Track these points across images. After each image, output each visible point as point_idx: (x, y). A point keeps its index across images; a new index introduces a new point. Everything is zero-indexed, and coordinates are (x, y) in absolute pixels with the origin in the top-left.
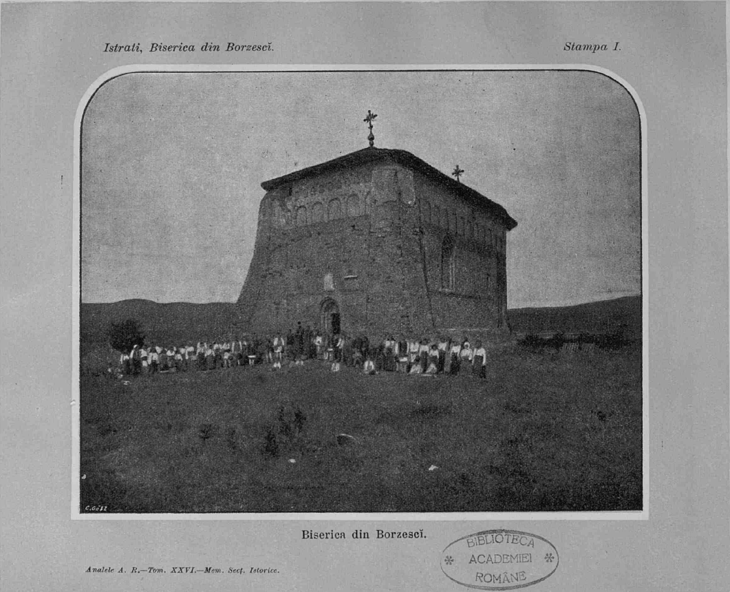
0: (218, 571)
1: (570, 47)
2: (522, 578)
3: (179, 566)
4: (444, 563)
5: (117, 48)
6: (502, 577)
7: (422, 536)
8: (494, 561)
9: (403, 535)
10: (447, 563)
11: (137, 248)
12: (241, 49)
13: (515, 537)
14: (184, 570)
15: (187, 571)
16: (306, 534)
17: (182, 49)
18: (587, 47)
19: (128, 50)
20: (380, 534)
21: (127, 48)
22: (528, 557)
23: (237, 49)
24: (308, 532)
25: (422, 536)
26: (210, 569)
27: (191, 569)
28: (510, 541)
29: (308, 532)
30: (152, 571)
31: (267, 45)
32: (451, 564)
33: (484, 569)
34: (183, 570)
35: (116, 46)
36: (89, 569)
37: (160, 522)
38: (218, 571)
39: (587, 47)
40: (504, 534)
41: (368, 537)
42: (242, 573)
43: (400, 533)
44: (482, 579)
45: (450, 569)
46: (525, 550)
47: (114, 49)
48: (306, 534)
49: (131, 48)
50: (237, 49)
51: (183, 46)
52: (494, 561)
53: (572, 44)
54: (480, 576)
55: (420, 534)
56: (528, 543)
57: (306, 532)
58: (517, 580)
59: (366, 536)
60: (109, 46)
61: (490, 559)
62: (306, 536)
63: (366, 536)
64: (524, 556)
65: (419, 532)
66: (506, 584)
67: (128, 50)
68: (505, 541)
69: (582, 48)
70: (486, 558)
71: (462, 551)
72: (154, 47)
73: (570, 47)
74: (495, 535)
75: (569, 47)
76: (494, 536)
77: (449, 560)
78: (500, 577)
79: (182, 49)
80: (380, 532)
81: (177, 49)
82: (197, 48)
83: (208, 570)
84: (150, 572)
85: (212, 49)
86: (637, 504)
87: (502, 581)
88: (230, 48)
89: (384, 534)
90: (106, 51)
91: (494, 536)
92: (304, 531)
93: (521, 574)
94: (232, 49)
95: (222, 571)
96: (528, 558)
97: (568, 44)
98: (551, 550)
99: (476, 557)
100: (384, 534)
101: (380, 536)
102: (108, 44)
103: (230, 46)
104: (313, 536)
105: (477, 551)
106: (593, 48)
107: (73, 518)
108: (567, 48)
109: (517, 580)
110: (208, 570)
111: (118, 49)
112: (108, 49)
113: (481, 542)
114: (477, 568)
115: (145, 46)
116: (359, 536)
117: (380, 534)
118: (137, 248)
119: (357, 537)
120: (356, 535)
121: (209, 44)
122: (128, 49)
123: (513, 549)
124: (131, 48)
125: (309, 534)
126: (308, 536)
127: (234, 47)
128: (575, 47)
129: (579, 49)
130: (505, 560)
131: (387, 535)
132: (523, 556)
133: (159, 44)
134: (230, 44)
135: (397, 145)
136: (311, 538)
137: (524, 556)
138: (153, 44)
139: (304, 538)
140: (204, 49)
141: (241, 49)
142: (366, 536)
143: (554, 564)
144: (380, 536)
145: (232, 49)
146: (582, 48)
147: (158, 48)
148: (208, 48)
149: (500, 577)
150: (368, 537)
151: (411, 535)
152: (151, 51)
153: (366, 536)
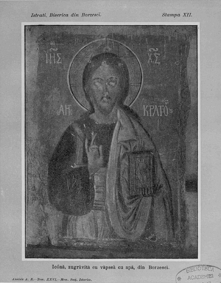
0: (66, 280)
1: (33, 15)
3: (50, 278)
5: (36, 15)
7: (167, 269)
8: (198, 278)
9: (160, 268)
10: (178, 280)
12: (88, 16)
13: (206, 268)
14: (52, 279)
15: (53, 280)
17: (63, 15)
18: (172, 15)
20: (150, 267)
23: (86, 16)
28: (204, 269)
30: (39, 279)
35: (36, 15)
38: (66, 280)
39: (172, 15)
41: (115, 269)
42: (76, 281)
46: (211, 273)
47: (35, 16)
49: (42, 15)
50: (86, 16)
51: (63, 14)
52: (198, 278)
53: (166, 14)
55: (167, 268)
56: (211, 269)
59: (143, 268)
60: (33, 14)
61: (196, 277)
63: (144, 268)
64: (210, 275)
65: (166, 267)
68: (202, 269)
69: (170, 15)
72: (51, 15)
73: (165, 15)
76: (197, 268)
79: (63, 15)
80: (150, 266)
81: (61, 16)
83: (62, 280)
84: (38, 280)
85: (76, 15)
88: (83, 16)
90: (32, 17)
91: (197, 268)
92: (149, 266)
94: (52, 16)
97: (164, 14)
99: (190, 277)
100: (152, 267)
101: (150, 268)
102: (33, 14)
103: (84, 15)
105: (190, 274)
106: (174, 15)
108: (163, 15)
110: (62, 280)
112: (33, 16)
113: (192, 270)
116: (140, 268)
117: (150, 267)
119: (140, 268)
120: (139, 267)
121: (167, 14)
122: (41, 16)
124: (42, 15)
127: (85, 15)
128: (167, 15)
132: (210, 275)
138: (83, 14)
140: (72, 16)
141: (88, 16)
142: (143, 268)
143: (178, 276)
144: (150, 268)
145: (52, 16)
146: (170, 15)
150: (144, 269)
152: (32, 17)
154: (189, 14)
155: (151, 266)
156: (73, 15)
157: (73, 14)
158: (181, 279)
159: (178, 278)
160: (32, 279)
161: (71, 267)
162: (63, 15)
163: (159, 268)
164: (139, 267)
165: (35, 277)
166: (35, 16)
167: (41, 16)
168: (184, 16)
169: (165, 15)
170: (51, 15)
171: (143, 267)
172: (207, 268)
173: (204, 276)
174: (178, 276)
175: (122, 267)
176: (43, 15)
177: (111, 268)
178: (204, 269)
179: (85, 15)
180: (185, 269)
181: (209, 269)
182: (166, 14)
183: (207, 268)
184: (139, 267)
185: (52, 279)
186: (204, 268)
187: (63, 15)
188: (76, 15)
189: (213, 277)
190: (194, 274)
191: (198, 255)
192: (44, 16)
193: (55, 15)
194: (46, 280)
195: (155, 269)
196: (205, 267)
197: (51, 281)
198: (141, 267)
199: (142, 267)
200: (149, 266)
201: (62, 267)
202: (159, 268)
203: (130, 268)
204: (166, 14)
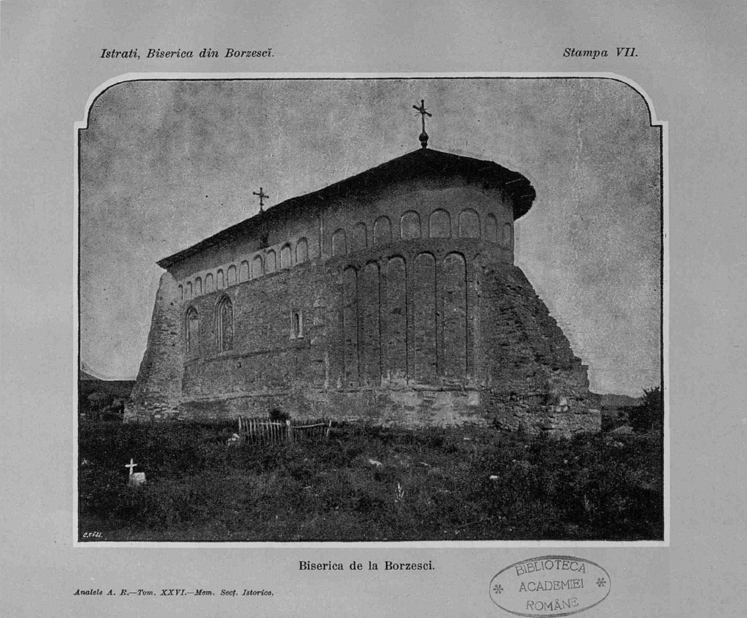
1: (570, 52)
2: (574, 604)
4: (493, 593)
6: (554, 604)
7: (430, 568)
8: (544, 588)
14: (174, 592)
16: (303, 565)
17: (180, 54)
18: (588, 53)
19: (203, 56)
22: (580, 583)
24: (305, 563)
25: (430, 568)
26: (201, 591)
29: (305, 563)
30: (142, 593)
32: (500, 592)
34: (173, 592)
35: (113, 52)
36: (78, 591)
37: (97, 549)
41: (342, 569)
43: (409, 565)
44: (533, 606)
48: (303, 565)
49: (129, 54)
52: (544, 588)
53: (572, 50)
56: (579, 567)
57: (303, 564)
58: (569, 607)
61: (540, 586)
62: (303, 567)
67: (203, 56)
70: (537, 586)
71: (510, 581)
73: (570, 52)
74: (545, 561)
77: (498, 589)
79: (180, 54)
80: (389, 563)
81: (175, 55)
82: (196, 54)
83: (199, 592)
84: (140, 594)
89: (392, 565)
90: (103, 57)
95: (154, 593)
96: (577, 584)
97: (568, 50)
100: (392, 565)
102: (105, 50)
104: (310, 567)
105: (526, 578)
106: (593, 54)
108: (566, 54)
109: (569, 607)
110: (199, 592)
111: (115, 54)
112: (106, 54)
114: (532, 596)
115: (143, 52)
117: (389, 566)
120: (355, 566)
121: (576, 50)
122: (125, 55)
124: (129, 54)
125: (307, 566)
126: (306, 568)
127: (233, 53)
128: (574, 53)
130: (576, 585)
131: (396, 567)
132: (576, 582)
133: (157, 50)
134: (229, 50)
135: (529, 174)
136: (309, 569)
138: (150, 50)
140: (202, 55)
144: (389, 567)
148: (206, 54)
151: (420, 567)
152: (103, 57)
154: (631, 50)
155: (391, 563)
156: (203, 54)
157: (205, 50)
159: (496, 586)
160: (123, 592)
163: (410, 566)
164: (353, 566)
167: (125, 55)
169: (571, 52)
172: (569, 565)
173: (560, 584)
176: (131, 52)
177: (318, 566)
178: (560, 567)
180: (512, 566)
181: (574, 566)
182: (573, 51)
183: (569, 565)
184: (353, 566)
185: (174, 592)
186: (561, 564)
189: (583, 587)
190: (536, 577)
191: (397, 542)
192: (133, 54)
193: (160, 54)
195: (401, 569)
196: (562, 561)
198: (309, 565)
200: (301, 562)
202: (410, 566)
204: (573, 51)
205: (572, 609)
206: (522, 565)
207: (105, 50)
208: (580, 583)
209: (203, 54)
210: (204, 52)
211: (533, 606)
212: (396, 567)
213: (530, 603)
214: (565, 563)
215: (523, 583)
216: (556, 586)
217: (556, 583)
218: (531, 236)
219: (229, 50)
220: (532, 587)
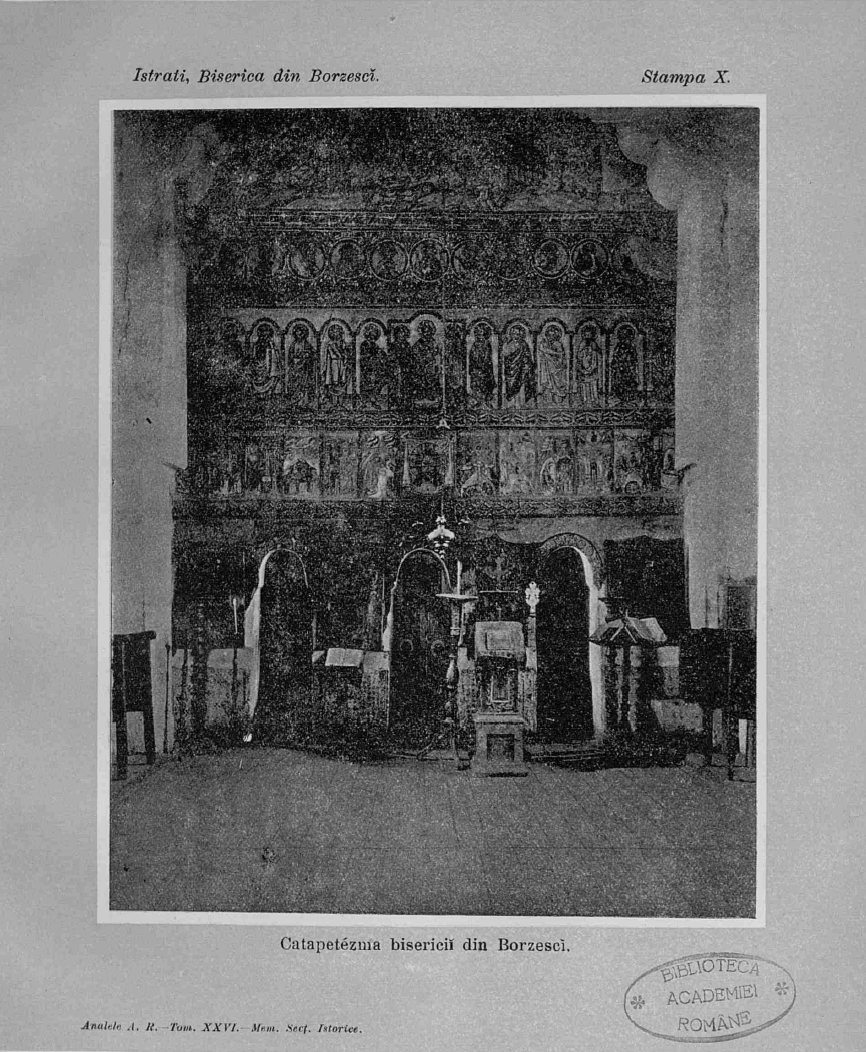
1: (141, 76)
5: (153, 75)
11: (406, 436)
12: (332, 78)
14: (222, 1028)
17: (246, 77)
18: (677, 78)
20: (505, 944)
21: (664, 77)
23: (326, 78)
27: (232, 1026)
31: (370, 72)
33: (685, 1011)
35: (151, 74)
40: (714, 959)
41: (485, 949)
44: (688, 1026)
45: (638, 1014)
47: (148, 77)
49: (173, 76)
50: (326, 78)
51: (247, 74)
54: (684, 1022)
55: (561, 945)
63: (483, 946)
66: (724, 1032)
69: (669, 79)
71: (653, 989)
73: (141, 76)
75: (650, 78)
78: (713, 1021)
79: (246, 77)
80: (504, 942)
83: (256, 1028)
85: (290, 78)
86: (120, 900)
87: (717, 1028)
89: (509, 944)
90: (136, 79)
91: (701, 963)
92: (501, 940)
93: (743, 1015)
96: (749, 992)
97: (649, 74)
98: (786, 979)
100: (509, 944)
102: (139, 69)
103: (316, 74)
104: (405, 946)
105: (676, 985)
106: (685, 79)
107: (763, 925)
108: (647, 79)
114: (685, 1011)
117: (505, 944)
118: (406, 436)
120: (467, 946)
121: (660, 75)
122: (168, 77)
123: (729, 980)
124: (173, 76)
127: (321, 76)
128: (658, 77)
129: (665, 81)
131: (514, 946)
136: (403, 949)
137: (747, 988)
139: (501, 949)
143: (790, 993)
144: (504, 947)
146: (669, 79)
147: (211, 79)
149: (713, 1021)
150: (485, 949)
153: (483, 946)
155: (507, 941)
156: (278, 78)
157: (282, 70)
158: (779, 984)
160: (150, 1027)
161: (357, 945)
162: (245, 76)
163: (535, 946)
165: (162, 1022)
166: (148, 77)
167: (168, 77)
168: (720, 80)
169: (653, 77)
170: (205, 76)
171: (480, 943)
172: (736, 964)
173: (724, 992)
174: (790, 993)
175: (393, 948)
179: (321, 76)
182: (656, 75)
183: (736, 964)
187: (245, 76)
188: (290, 78)
193: (217, 77)
194: (199, 1029)
195: (425, 949)
196: (726, 959)
197: (216, 1032)
199: (478, 945)
201: (367, 946)
202: (535, 946)
203: (321, 945)
205: (743, 1029)
206: (670, 967)
207: (139, 69)
208: (752, 991)
209: (278, 78)
210: (687, 80)
211: (688, 1026)
212: (514, 946)
213: (683, 1021)
214: (731, 962)
215: (672, 994)
216: (720, 996)
217: (720, 991)
218: (478, 813)
219: (315, 71)
220: (685, 997)
